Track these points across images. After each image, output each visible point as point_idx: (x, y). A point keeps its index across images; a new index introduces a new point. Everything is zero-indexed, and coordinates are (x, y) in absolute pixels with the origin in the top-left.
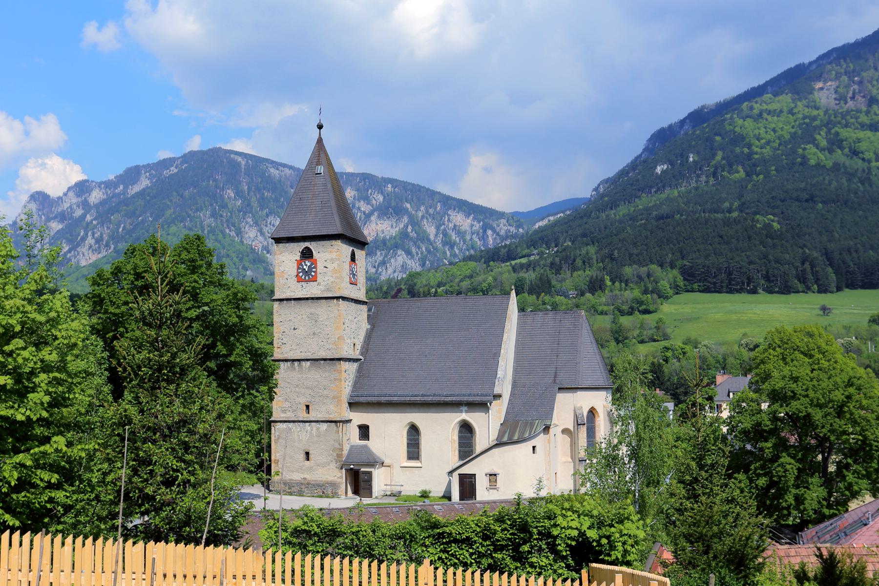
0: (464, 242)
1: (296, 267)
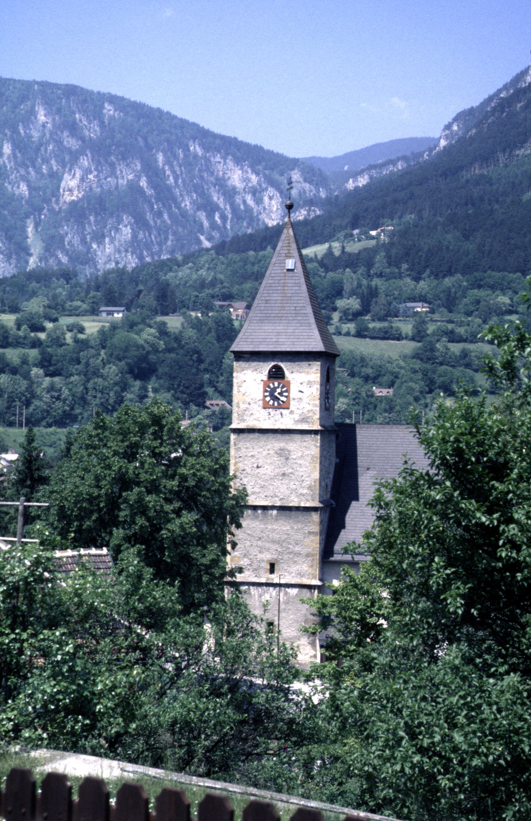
0: (232, 666)
1: (262, 389)
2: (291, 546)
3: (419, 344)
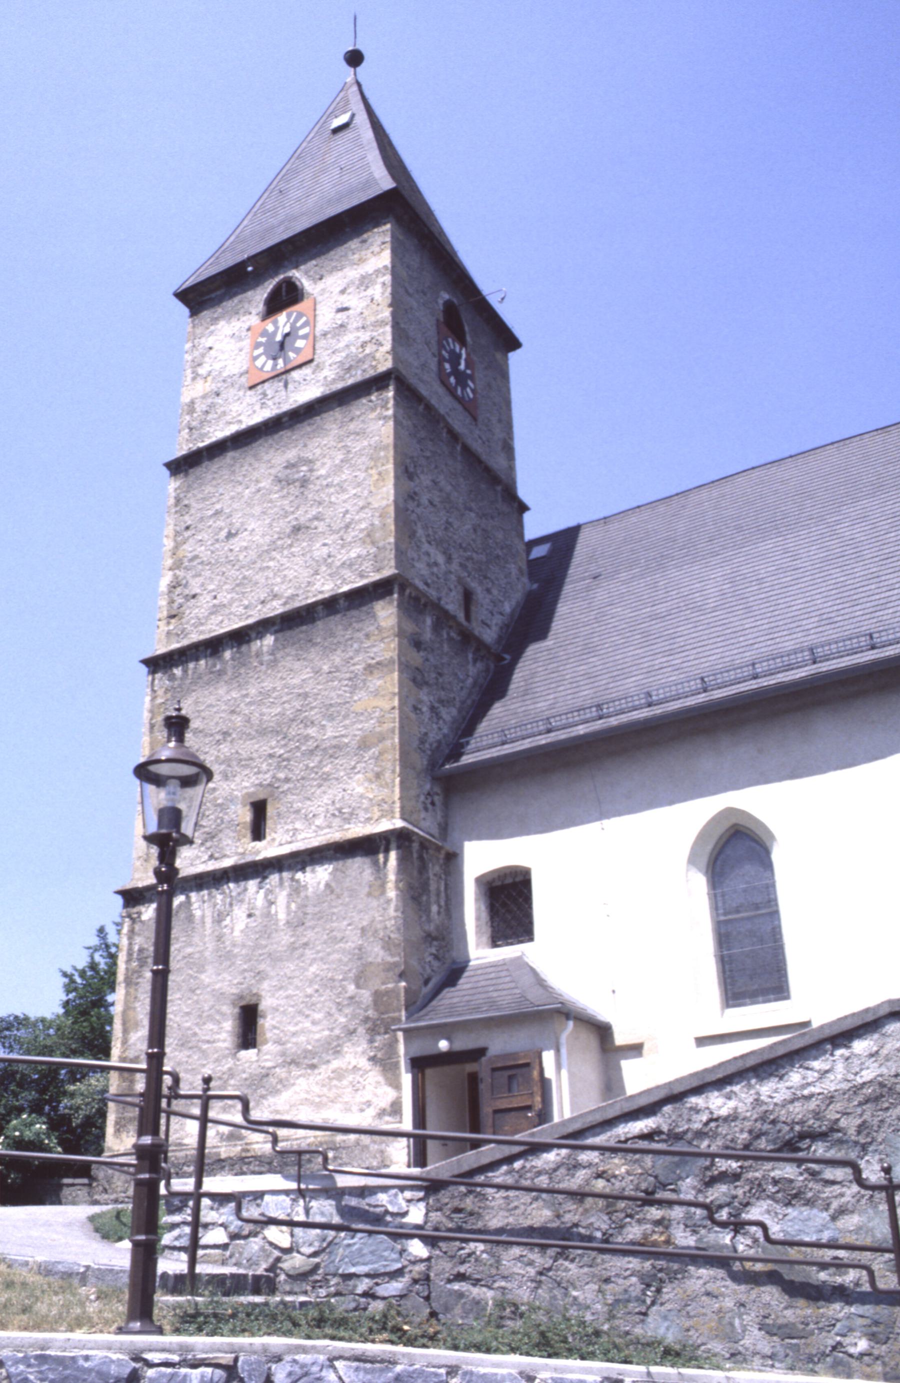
2: (312, 731)
3: (387, 1036)
